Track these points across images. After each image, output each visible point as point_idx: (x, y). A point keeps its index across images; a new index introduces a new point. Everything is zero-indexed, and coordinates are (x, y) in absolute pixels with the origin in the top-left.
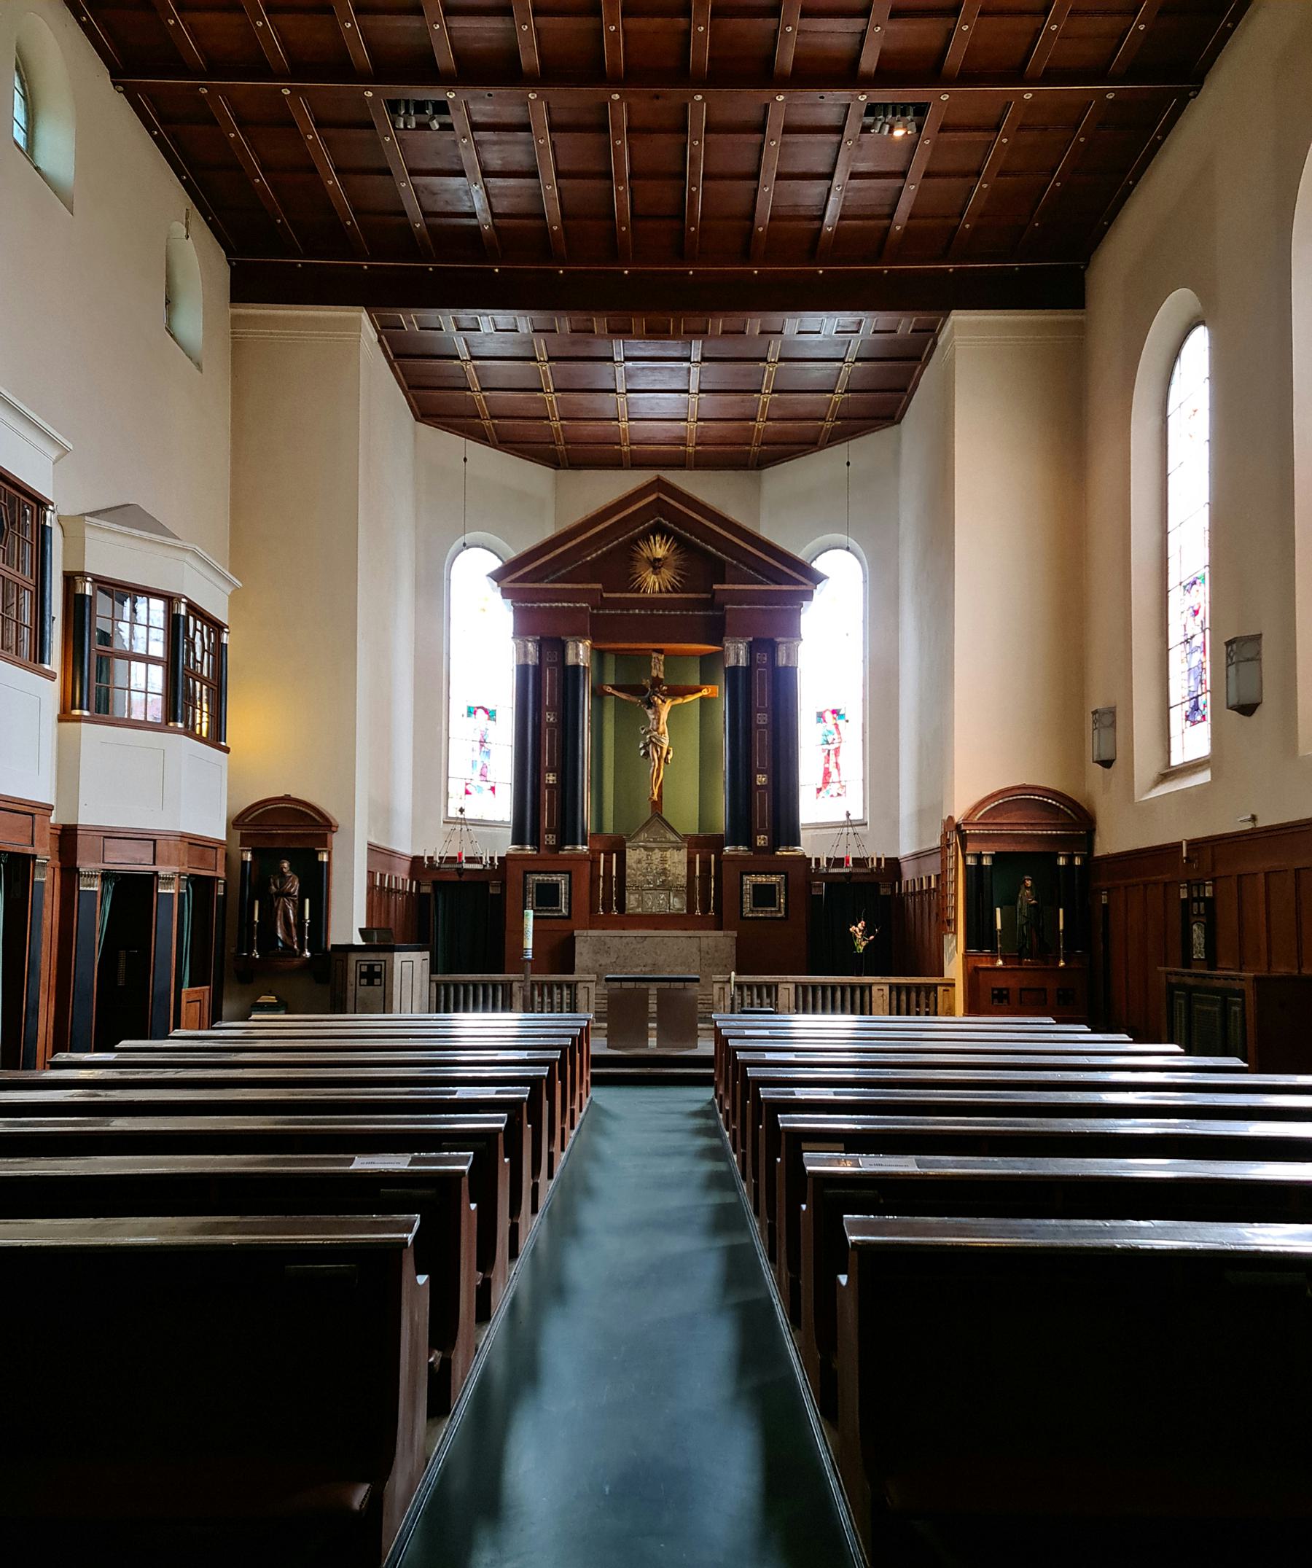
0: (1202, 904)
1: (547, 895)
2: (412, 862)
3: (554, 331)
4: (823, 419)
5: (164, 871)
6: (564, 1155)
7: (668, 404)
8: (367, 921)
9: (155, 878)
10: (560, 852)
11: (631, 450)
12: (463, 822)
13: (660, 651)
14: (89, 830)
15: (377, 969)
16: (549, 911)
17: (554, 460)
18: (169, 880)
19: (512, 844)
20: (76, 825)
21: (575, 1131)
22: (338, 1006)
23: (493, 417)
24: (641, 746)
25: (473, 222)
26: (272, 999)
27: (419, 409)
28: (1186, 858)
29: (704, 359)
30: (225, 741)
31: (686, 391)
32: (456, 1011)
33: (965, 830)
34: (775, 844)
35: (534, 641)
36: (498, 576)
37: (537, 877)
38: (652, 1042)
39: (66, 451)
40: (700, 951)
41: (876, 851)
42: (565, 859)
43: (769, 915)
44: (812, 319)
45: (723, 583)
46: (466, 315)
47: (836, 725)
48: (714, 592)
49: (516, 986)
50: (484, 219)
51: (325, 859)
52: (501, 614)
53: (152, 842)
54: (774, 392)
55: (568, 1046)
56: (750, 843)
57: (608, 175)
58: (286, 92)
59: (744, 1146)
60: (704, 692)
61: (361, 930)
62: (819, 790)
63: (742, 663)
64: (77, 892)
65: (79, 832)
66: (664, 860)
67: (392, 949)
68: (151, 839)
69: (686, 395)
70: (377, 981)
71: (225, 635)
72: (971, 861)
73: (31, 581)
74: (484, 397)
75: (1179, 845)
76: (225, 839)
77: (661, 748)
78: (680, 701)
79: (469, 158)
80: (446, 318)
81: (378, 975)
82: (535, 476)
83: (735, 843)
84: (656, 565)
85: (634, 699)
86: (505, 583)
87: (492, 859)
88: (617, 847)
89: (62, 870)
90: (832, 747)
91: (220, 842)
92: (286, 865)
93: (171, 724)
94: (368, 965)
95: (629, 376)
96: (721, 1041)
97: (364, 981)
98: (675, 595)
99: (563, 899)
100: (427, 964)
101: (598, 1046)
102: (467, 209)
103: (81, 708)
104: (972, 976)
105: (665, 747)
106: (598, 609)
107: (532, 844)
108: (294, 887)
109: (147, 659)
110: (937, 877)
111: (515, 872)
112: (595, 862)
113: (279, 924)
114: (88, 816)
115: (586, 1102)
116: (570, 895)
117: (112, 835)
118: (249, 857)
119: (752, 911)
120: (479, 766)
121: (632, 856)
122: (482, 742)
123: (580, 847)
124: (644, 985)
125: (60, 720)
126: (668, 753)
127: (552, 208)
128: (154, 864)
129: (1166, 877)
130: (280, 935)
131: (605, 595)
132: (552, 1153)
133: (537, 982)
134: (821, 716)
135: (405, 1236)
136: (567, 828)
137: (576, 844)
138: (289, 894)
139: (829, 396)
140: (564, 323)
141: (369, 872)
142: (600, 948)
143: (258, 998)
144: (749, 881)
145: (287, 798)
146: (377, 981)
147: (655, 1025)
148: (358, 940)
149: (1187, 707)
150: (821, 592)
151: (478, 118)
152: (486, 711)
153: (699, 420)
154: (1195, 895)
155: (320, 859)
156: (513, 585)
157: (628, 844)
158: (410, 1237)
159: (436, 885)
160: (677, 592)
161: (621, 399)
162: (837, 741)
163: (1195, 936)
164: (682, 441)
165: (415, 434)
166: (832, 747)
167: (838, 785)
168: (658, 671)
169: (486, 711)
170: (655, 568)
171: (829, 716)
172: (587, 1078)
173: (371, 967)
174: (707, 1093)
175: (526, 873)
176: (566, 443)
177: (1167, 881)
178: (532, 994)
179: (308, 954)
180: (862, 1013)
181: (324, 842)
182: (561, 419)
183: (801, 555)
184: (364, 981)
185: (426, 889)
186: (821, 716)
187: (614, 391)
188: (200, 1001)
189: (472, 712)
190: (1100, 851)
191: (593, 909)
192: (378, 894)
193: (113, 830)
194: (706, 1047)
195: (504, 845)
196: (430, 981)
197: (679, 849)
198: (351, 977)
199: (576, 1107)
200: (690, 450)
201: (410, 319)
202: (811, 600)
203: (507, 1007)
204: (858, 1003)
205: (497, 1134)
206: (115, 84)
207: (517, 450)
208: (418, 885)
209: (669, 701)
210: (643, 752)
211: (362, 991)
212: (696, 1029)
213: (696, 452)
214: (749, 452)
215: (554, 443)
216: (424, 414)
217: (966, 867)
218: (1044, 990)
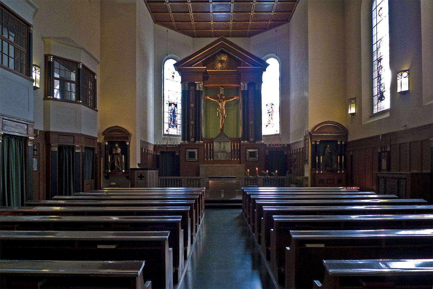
0: (386, 153)
2: (154, 146)
7: (222, 15)
8: (141, 162)
9: (74, 148)
10: (195, 143)
11: (214, 31)
12: (169, 135)
15: (143, 175)
16: (192, 159)
17: (193, 36)
19: (182, 141)
20: (50, 131)
23: (175, 21)
24: (217, 113)
26: (114, 183)
27: (155, 19)
28: (381, 139)
30: (96, 108)
31: (230, 12)
33: (312, 134)
34: (256, 140)
37: (189, 150)
38: (223, 196)
40: (235, 170)
41: (285, 142)
42: (198, 145)
43: (254, 160)
45: (240, 66)
47: (272, 108)
51: (128, 144)
53: (73, 137)
54: (254, 12)
55: (197, 198)
56: (248, 140)
60: (235, 98)
61: (138, 164)
64: (27, 146)
65: (50, 133)
66: (389, 147)
67: (147, 169)
72: (313, 143)
73: (25, 50)
74: (173, 15)
75: (379, 136)
77: (223, 114)
78: (228, 101)
81: (143, 177)
82: (188, 39)
84: (222, 62)
88: (211, 141)
89: (46, 145)
90: (270, 114)
93: (78, 101)
94: (141, 174)
95: (214, 7)
96: (244, 193)
97: (139, 178)
103: (50, 96)
104: (313, 175)
105: (224, 114)
106: (205, 74)
107: (187, 141)
109: (71, 82)
113: (116, 162)
116: (198, 155)
117: (61, 134)
118: (107, 143)
123: (200, 142)
126: (225, 115)
128: (74, 143)
130: (116, 165)
131: (207, 70)
132: (192, 235)
133: (189, 179)
135: (166, 237)
136: (198, 137)
139: (270, 13)
141: (141, 148)
143: (111, 183)
145: (117, 127)
147: (223, 191)
148: (138, 167)
150: (268, 69)
152: (174, 104)
153: (234, 12)
155: (126, 144)
157: (214, 140)
158: (167, 237)
160: (227, 69)
162: (272, 112)
163: (383, 163)
167: (272, 124)
168: (222, 92)
169: (174, 104)
170: (221, 63)
173: (141, 175)
174: (241, 211)
175: (186, 149)
176: (196, 29)
177: (373, 147)
178: (188, 183)
182: (194, 22)
184: (139, 178)
185: (158, 154)
187: (209, 12)
188: (91, 184)
190: (349, 140)
192: (144, 154)
194: (240, 198)
195: (179, 141)
196: (159, 179)
197: (228, 142)
198: (136, 177)
200: (230, 31)
202: (265, 71)
205: (193, 204)
207: (182, 32)
208: (156, 152)
210: (218, 115)
211: (140, 181)
213: (232, 32)
215: (192, 29)
217: (312, 145)
218: (334, 179)
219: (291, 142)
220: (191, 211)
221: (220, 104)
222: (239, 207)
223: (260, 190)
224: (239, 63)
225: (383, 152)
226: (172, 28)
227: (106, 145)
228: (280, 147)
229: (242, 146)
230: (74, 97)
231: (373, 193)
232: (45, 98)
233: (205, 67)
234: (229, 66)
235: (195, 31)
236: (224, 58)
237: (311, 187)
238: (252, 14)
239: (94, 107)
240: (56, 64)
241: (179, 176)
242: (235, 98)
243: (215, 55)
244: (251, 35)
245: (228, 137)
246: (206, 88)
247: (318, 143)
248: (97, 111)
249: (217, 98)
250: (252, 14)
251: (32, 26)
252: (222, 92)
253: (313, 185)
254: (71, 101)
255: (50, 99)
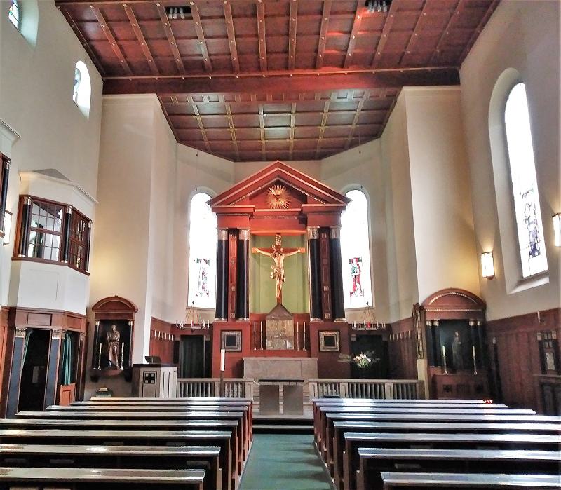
0: (550, 343)
1: (231, 341)
3: (234, 101)
4: (347, 137)
5: (55, 328)
6: (240, 478)
7: (280, 132)
12: (193, 309)
13: (279, 234)
14: (22, 309)
18: (57, 333)
21: (245, 462)
22: (135, 393)
25: (200, 58)
26: (106, 390)
29: (297, 112)
32: (189, 396)
34: (334, 317)
35: (226, 230)
36: (210, 203)
37: (227, 333)
38: (281, 410)
39: (18, 138)
41: (383, 321)
42: (241, 324)
44: (342, 93)
45: (306, 203)
46: (198, 96)
47: (358, 265)
48: (302, 208)
49: (217, 384)
50: (206, 58)
52: (212, 218)
56: (322, 317)
57: (256, 36)
58: (125, 5)
59: (341, 475)
60: (299, 251)
62: (351, 294)
63: (315, 238)
66: (283, 325)
67: (159, 366)
68: (50, 314)
69: (289, 128)
70: (152, 381)
71: (90, 224)
76: (85, 314)
78: (288, 255)
79: (199, 32)
80: (189, 97)
81: (153, 378)
83: (315, 317)
85: (268, 254)
86: (213, 206)
87: (206, 325)
91: (83, 316)
92: (114, 327)
96: (316, 409)
97: (147, 381)
98: (286, 210)
99: (238, 343)
100: (176, 373)
101: (256, 413)
102: (198, 53)
103: (22, 254)
107: (224, 318)
108: (117, 337)
110: (411, 332)
111: (216, 331)
112: (252, 326)
114: (22, 303)
115: (251, 443)
117: (32, 312)
118: (98, 324)
119: (324, 348)
120: (202, 284)
121: (269, 323)
122: (203, 274)
124: (275, 384)
125: (13, 259)
127: (234, 51)
129: (529, 330)
134: (350, 261)
136: (240, 311)
137: (221, 317)
138: (114, 341)
140: (239, 98)
141: (151, 330)
142: (255, 365)
144: (323, 334)
146: (152, 381)
148: (145, 362)
149: (530, 249)
150: (349, 206)
151: (204, 15)
154: (549, 338)
156: (217, 207)
159: (183, 337)
161: (262, 131)
164: (288, 148)
165: (176, 151)
166: (356, 274)
168: (278, 242)
171: (354, 261)
172: (251, 431)
174: (311, 438)
175: (222, 331)
179: (122, 368)
180: (376, 398)
181: (131, 316)
183: (340, 192)
185: (178, 339)
186: (350, 261)
189: (198, 261)
191: (252, 347)
193: (33, 309)
194: (308, 414)
197: (290, 319)
198: (141, 379)
199: (246, 448)
201: (175, 98)
203: (212, 395)
204: (378, 393)
205: (199, 485)
206: (56, 6)
209: (283, 255)
210: (272, 277)
211: (147, 386)
212: (302, 406)
214: (315, 152)
216: (181, 139)
219: (393, 320)
220: (233, 438)
221: (276, 260)
222: (310, 432)
223: (343, 404)
224: (304, 199)
225: (546, 340)
226: (205, 150)
227: (96, 327)
228: (375, 329)
229: (311, 327)
230: (56, 256)
231: (530, 411)
232: (15, 258)
233: (253, 206)
234: (289, 205)
235: (235, 142)
236: (279, 191)
237: (430, 399)
238: (323, 128)
239: (84, 269)
240: (35, 209)
241: (211, 377)
242: (299, 251)
243: (267, 188)
244: (322, 156)
245: (289, 313)
246: (254, 236)
247: (436, 324)
248: (88, 274)
249: (270, 251)
250: (325, 115)
251: (10, 160)
252: (278, 242)
253: (434, 395)
254: (50, 262)
255: (21, 259)
